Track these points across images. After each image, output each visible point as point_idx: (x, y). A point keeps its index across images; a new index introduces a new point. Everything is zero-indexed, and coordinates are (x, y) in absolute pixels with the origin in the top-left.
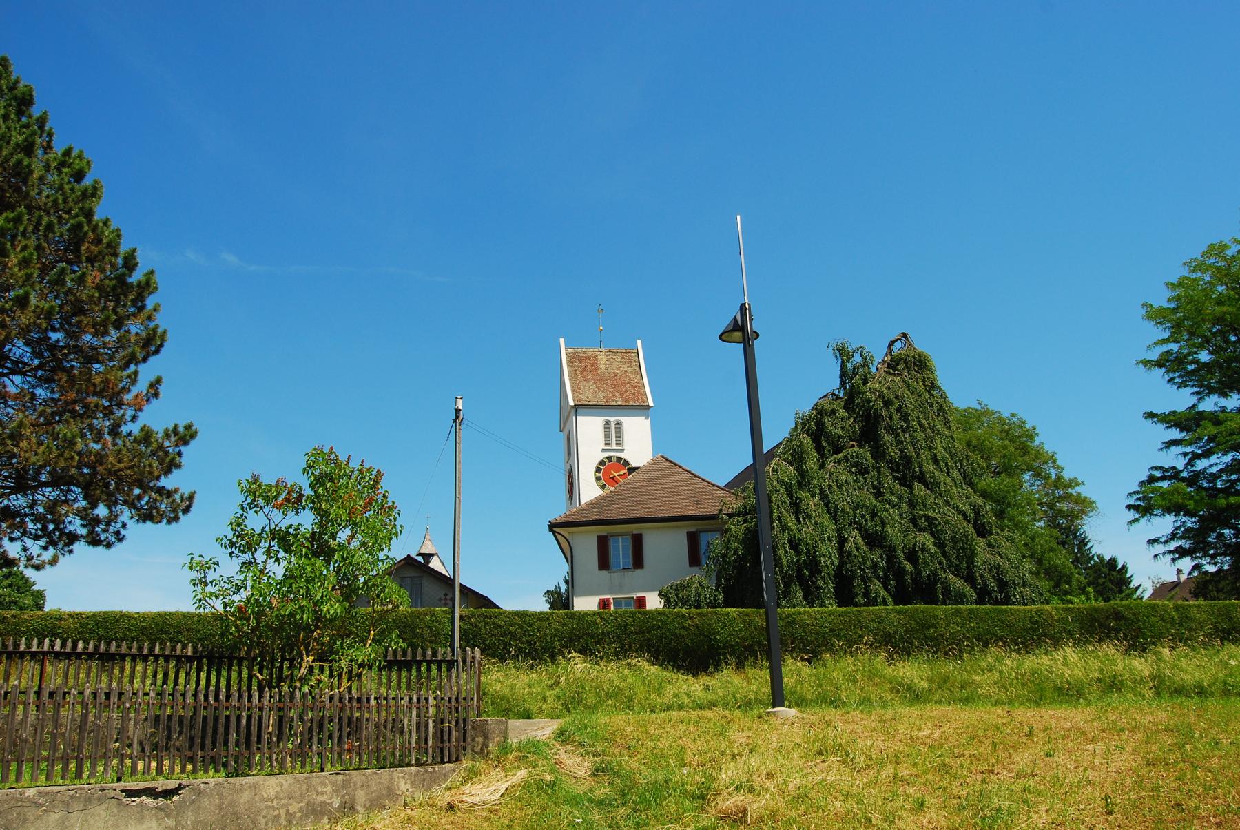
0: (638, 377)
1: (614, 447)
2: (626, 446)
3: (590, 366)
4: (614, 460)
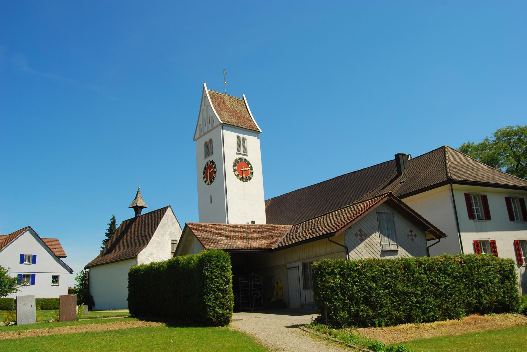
0: (248, 115)
1: (242, 153)
2: (249, 152)
3: (222, 103)
4: (243, 161)
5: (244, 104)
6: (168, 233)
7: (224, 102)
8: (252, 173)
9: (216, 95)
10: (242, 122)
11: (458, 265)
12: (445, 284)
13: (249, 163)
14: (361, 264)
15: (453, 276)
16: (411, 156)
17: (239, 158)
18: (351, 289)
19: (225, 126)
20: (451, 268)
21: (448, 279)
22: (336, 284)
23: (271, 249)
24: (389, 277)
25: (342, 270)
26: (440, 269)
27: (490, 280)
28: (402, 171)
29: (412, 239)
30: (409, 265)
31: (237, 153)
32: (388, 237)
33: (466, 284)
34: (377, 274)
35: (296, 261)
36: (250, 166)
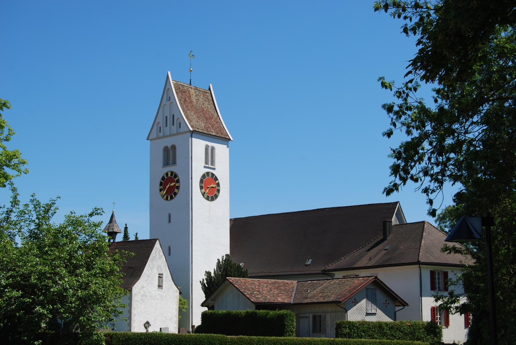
0: (216, 114)
2: (217, 165)
3: (187, 99)
4: (210, 175)
5: (210, 98)
6: (156, 266)
7: (190, 97)
8: (218, 191)
9: (181, 87)
10: (210, 126)
11: (408, 327)
12: (399, 336)
13: (216, 179)
14: (358, 324)
15: (404, 333)
16: (399, 204)
17: (206, 173)
18: (353, 335)
19: (195, 133)
20: (404, 328)
21: (401, 334)
22: (346, 332)
23: (291, 303)
24: (371, 331)
25: (350, 326)
26: (397, 329)
27: (425, 336)
28: (387, 237)
29: (386, 306)
30: (382, 325)
31: (205, 167)
32: (372, 302)
33: (411, 338)
34: (366, 329)
35: (308, 313)
36: (217, 182)
